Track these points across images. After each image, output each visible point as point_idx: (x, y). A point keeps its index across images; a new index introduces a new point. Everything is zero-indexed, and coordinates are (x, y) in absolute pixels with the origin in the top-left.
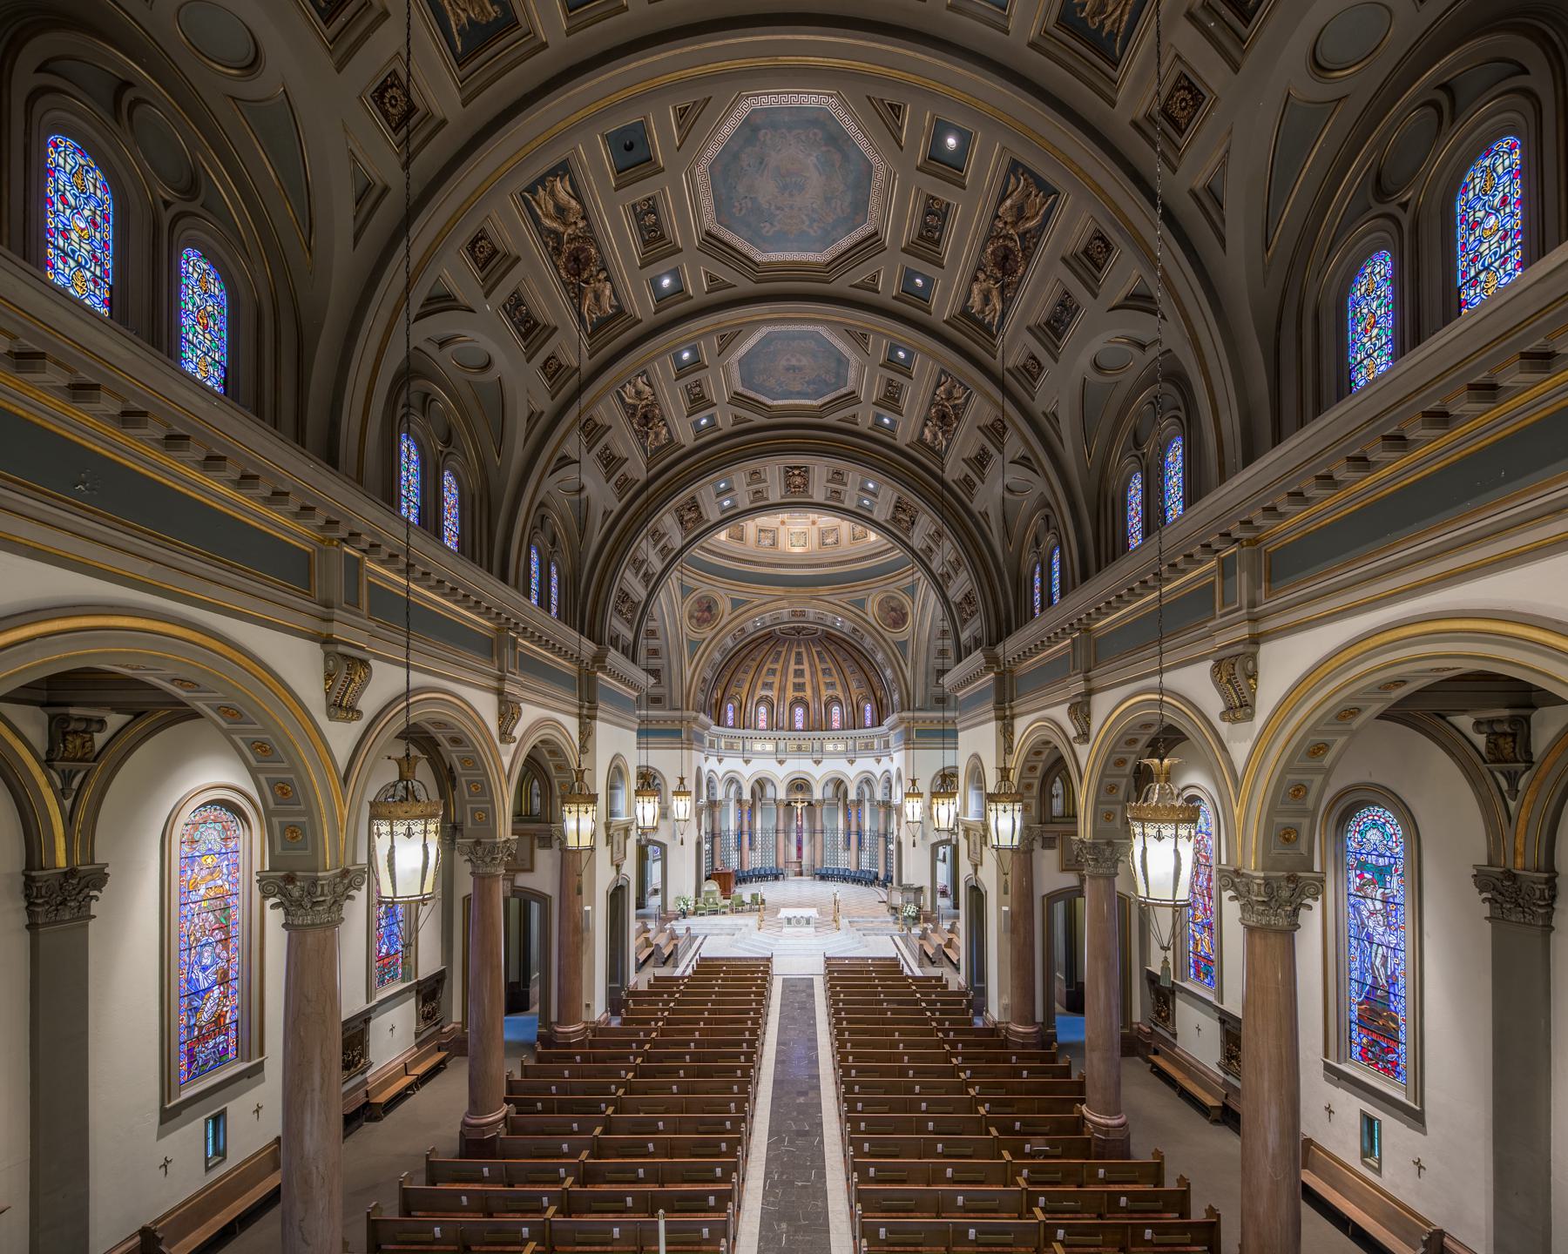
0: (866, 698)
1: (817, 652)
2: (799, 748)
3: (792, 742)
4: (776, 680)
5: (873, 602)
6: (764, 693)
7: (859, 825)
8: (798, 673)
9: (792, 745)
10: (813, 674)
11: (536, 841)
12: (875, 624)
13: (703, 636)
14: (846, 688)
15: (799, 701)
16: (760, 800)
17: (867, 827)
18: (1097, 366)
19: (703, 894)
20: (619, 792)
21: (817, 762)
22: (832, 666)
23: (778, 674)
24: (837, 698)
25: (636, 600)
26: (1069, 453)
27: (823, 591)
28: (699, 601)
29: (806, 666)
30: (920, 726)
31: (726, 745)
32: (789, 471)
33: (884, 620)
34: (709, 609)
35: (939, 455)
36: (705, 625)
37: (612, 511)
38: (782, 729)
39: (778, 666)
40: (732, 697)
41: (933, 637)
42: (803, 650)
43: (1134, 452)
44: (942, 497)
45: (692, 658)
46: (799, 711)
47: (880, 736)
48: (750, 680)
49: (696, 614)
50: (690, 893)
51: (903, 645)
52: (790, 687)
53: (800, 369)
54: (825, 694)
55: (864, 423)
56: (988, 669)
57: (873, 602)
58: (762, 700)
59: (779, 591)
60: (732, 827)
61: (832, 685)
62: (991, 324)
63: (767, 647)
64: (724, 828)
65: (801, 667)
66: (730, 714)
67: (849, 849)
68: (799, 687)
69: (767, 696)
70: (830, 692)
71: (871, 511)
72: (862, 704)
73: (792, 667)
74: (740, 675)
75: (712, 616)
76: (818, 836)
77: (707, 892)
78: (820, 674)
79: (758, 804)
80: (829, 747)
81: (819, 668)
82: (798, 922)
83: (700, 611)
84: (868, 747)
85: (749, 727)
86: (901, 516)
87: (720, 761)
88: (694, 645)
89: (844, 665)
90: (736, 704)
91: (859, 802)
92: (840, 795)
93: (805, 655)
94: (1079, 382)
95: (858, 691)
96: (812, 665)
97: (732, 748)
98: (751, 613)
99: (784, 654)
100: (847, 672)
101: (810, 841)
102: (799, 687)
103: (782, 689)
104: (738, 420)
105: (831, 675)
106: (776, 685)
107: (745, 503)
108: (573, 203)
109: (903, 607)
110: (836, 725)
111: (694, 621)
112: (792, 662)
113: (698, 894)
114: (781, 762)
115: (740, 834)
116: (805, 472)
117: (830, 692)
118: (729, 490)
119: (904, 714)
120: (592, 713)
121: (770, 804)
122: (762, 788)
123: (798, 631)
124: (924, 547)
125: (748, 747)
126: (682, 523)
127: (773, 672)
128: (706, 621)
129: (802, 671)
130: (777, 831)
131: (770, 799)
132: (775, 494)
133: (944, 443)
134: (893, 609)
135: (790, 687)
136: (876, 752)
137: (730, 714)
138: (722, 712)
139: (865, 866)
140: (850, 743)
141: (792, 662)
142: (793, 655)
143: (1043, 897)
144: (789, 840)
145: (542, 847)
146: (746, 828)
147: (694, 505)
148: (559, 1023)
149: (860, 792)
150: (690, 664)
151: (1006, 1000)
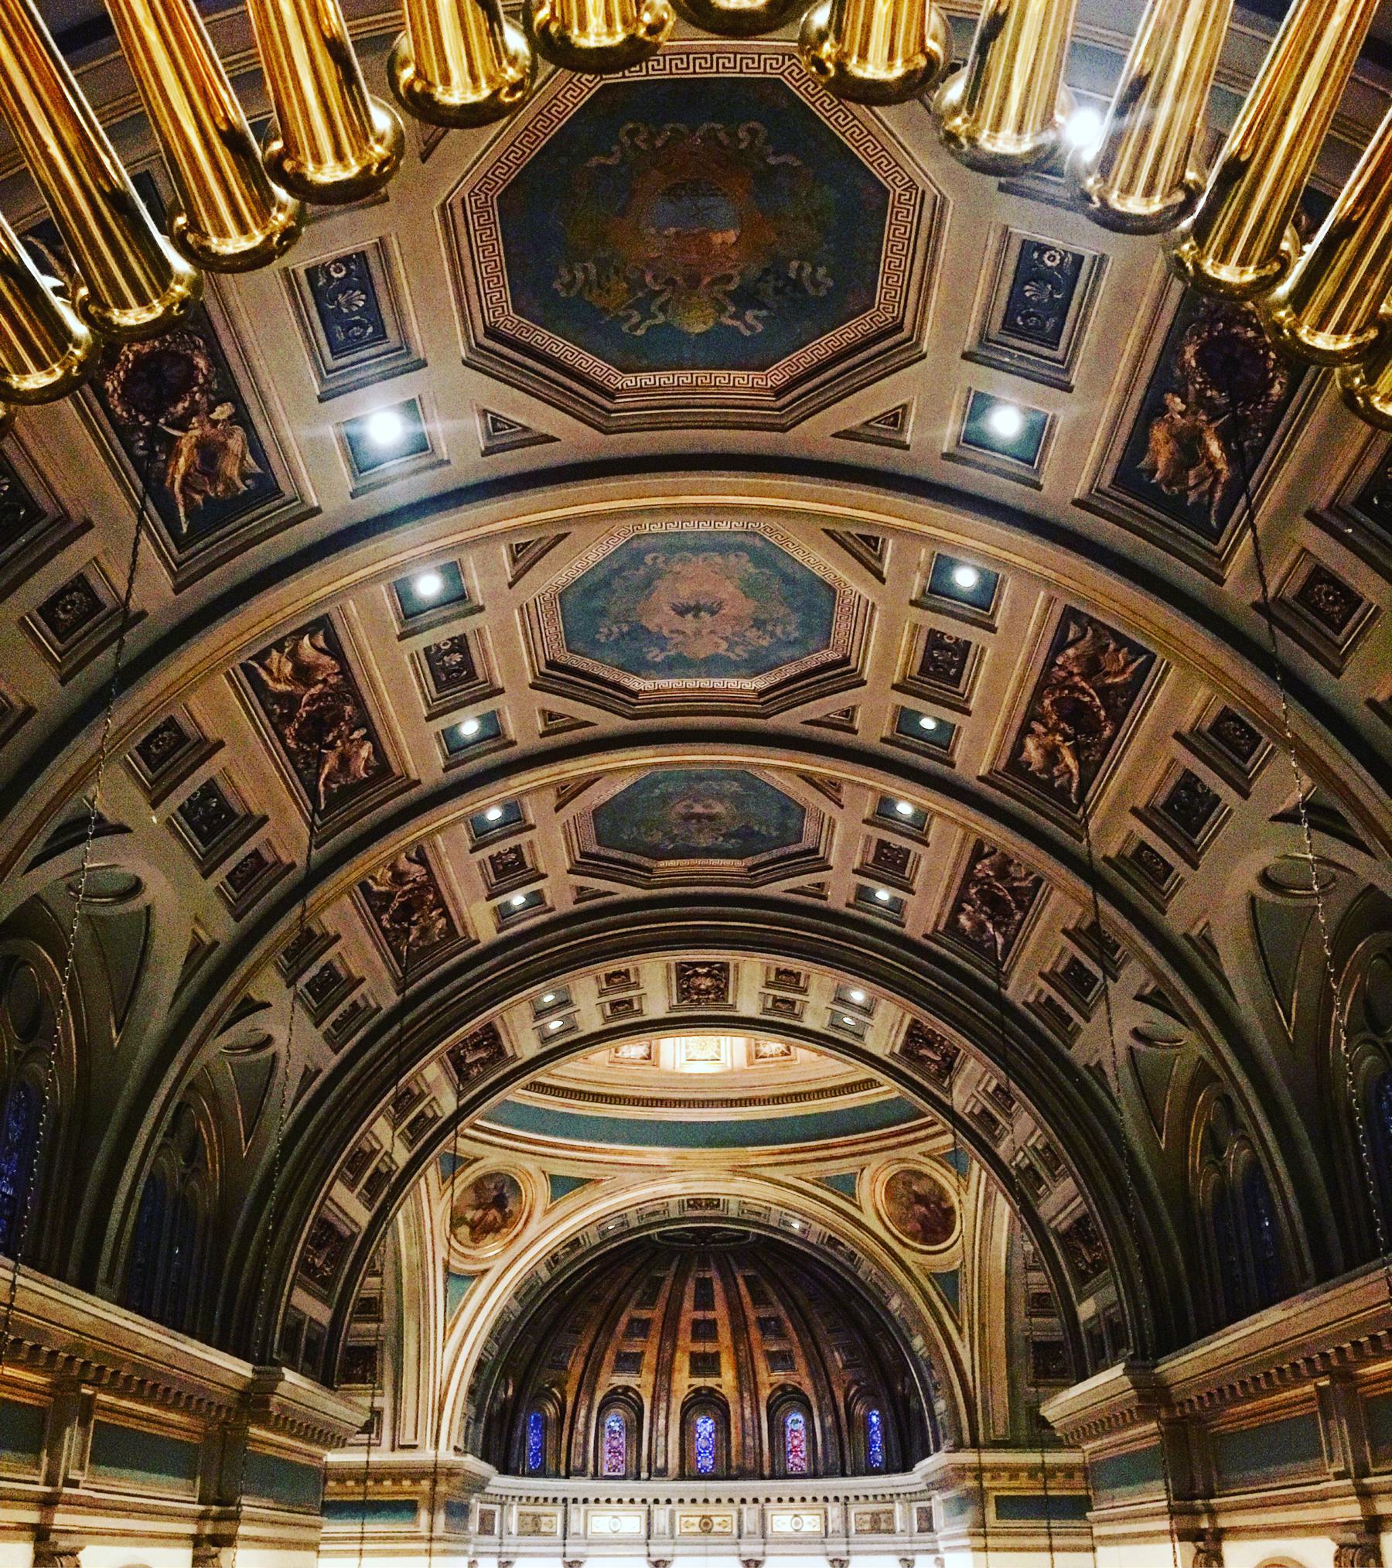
1: (746, 1279)
2: (706, 1524)
3: (688, 1508)
5: (874, 1180)
6: (620, 1380)
8: (705, 1330)
9: (688, 1519)
10: (739, 1330)
14: (819, 1369)
15: (704, 1401)
18: (1265, 879)
22: (783, 1313)
24: (796, 1390)
26: (1247, 1009)
28: (478, 1185)
29: (720, 1313)
30: (1002, 1487)
31: (522, 1523)
32: (685, 972)
33: (900, 1222)
34: (500, 1202)
35: (998, 964)
37: (319, 1071)
38: (662, 1473)
39: (655, 1314)
41: (1018, 1263)
42: (712, 1274)
43: (1368, 1034)
44: (1002, 1025)
46: (705, 1426)
47: (911, 1497)
48: (585, 1347)
49: (470, 1215)
51: (948, 1283)
52: (682, 1362)
53: (711, 818)
54: (769, 1379)
55: (839, 894)
56: (1146, 1411)
57: (874, 1180)
58: (619, 1397)
62: (1065, 790)
63: (628, 1271)
65: (710, 1315)
69: (627, 1389)
70: (779, 1377)
71: (861, 1037)
72: (859, 1410)
73: (689, 1313)
78: (755, 1334)
80: (781, 1522)
81: (751, 1315)
84: (879, 1524)
85: (581, 1472)
86: (923, 1052)
93: (717, 1287)
94: (1242, 908)
95: (848, 1376)
96: (735, 1309)
97: (537, 1532)
99: (668, 1282)
100: (821, 1330)
104: (582, 894)
105: (781, 1335)
106: (650, 1359)
107: (591, 1021)
108: (325, 660)
109: (942, 1195)
110: (798, 1460)
111: (464, 1231)
112: (688, 1304)
116: (720, 969)
117: (779, 1377)
118: (566, 1003)
120: (225, 1528)
124: (976, 1111)
125: (575, 1525)
126: (459, 1072)
127: (640, 1328)
128: (493, 1229)
129: (713, 1324)
132: (657, 1002)
133: (1000, 940)
134: (920, 1199)
135: (682, 1362)
136: (900, 1541)
140: (835, 1510)
142: (690, 1288)
147: (490, 1037)
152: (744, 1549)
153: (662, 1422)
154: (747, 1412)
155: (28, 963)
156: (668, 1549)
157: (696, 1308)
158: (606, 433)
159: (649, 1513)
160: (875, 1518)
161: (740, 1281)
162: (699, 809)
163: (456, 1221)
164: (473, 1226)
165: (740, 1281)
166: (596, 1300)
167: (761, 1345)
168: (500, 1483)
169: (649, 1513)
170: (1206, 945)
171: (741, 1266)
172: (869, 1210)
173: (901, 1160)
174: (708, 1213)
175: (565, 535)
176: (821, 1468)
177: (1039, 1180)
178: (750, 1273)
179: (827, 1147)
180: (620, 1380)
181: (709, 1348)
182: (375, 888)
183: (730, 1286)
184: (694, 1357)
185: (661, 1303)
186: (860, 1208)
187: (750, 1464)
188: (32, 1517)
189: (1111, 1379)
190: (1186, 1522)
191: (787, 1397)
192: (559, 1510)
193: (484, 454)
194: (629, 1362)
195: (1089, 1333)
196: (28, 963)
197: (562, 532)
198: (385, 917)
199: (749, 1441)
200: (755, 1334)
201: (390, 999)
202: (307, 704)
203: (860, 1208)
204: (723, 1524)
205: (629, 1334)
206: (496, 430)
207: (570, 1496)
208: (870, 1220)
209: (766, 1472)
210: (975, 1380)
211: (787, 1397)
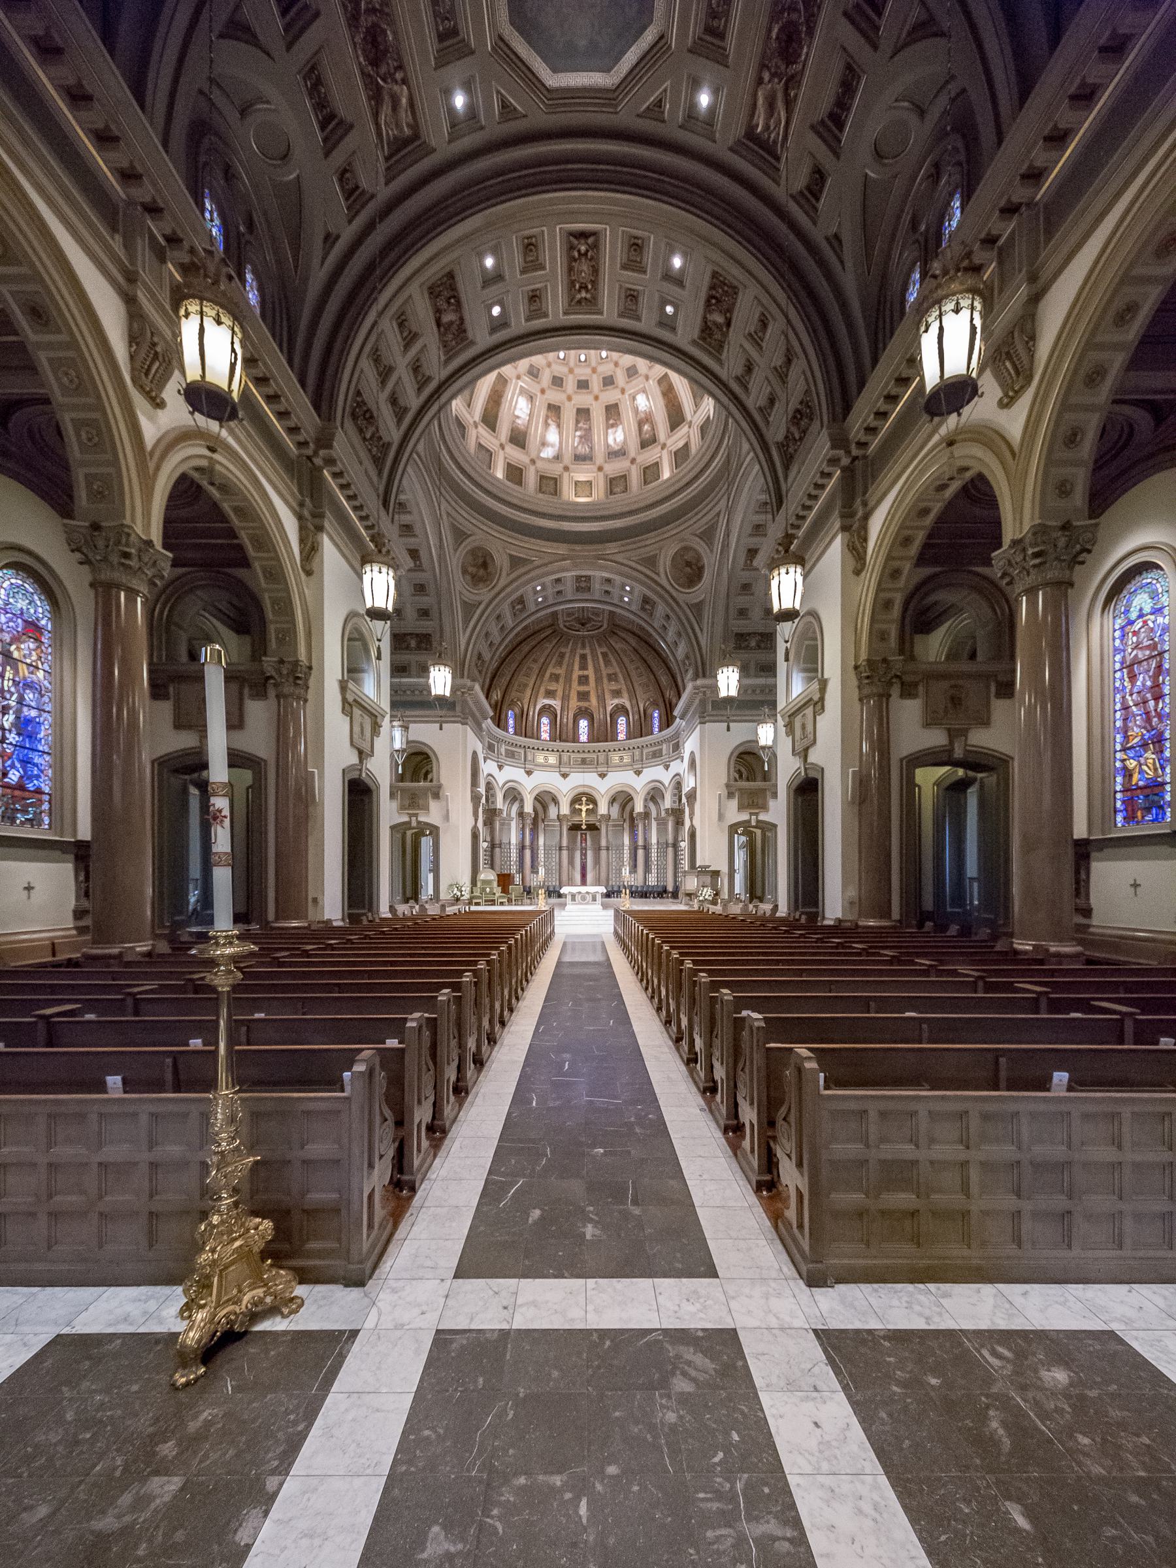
0: (655, 704)
4: (559, 688)
6: (547, 701)
7: (645, 839)
8: (584, 680)
10: (599, 680)
11: (246, 691)
12: (669, 587)
13: (478, 598)
14: (633, 695)
16: (543, 821)
17: (654, 840)
19: (479, 884)
20: (365, 675)
21: (603, 776)
22: (618, 670)
23: (562, 680)
24: (623, 707)
25: (386, 439)
27: (612, 548)
28: (474, 552)
29: (590, 672)
34: (485, 565)
36: (481, 585)
39: (560, 671)
40: (512, 704)
42: (587, 651)
45: (466, 621)
46: (583, 724)
49: (470, 569)
50: (465, 879)
52: (574, 696)
54: (611, 703)
59: (562, 549)
60: (514, 841)
61: (617, 693)
64: (505, 841)
65: (586, 673)
66: (511, 722)
67: (635, 872)
68: (584, 696)
69: (550, 706)
70: (616, 701)
71: (673, 329)
72: (649, 711)
73: (577, 673)
74: (521, 678)
75: (489, 574)
76: (603, 853)
77: (484, 882)
78: (605, 681)
79: (541, 826)
82: (584, 898)
83: (474, 566)
84: (657, 754)
87: (500, 767)
88: (469, 608)
89: (631, 667)
90: (517, 710)
91: (646, 815)
92: (626, 815)
93: (589, 658)
96: (597, 670)
98: (533, 574)
99: (567, 655)
101: (594, 867)
102: (584, 696)
103: (568, 680)
105: (616, 681)
106: (560, 693)
111: (468, 577)
112: (576, 666)
113: (474, 882)
114: (565, 776)
115: (522, 848)
117: (616, 701)
119: (699, 682)
122: (545, 808)
123: (583, 620)
125: (530, 757)
127: (555, 678)
129: (587, 677)
130: (560, 849)
131: (553, 820)
134: (688, 564)
135: (574, 696)
137: (511, 722)
138: (503, 717)
139: (652, 881)
140: (637, 752)
141: (576, 666)
142: (577, 659)
143: (901, 760)
144: (573, 867)
145: (253, 697)
146: (527, 842)
148: (277, 919)
150: (465, 630)
151: (853, 892)
164: (473, 576)
166: (535, 661)
167: (608, 686)
171: (600, 646)
172: (663, 575)
180: (547, 701)
183: (594, 656)
184: (579, 693)
185: (564, 666)
191: (621, 710)
192: (522, 751)
194: (550, 694)
200: (605, 681)
208: (664, 583)
210: (726, 497)
211: (621, 710)
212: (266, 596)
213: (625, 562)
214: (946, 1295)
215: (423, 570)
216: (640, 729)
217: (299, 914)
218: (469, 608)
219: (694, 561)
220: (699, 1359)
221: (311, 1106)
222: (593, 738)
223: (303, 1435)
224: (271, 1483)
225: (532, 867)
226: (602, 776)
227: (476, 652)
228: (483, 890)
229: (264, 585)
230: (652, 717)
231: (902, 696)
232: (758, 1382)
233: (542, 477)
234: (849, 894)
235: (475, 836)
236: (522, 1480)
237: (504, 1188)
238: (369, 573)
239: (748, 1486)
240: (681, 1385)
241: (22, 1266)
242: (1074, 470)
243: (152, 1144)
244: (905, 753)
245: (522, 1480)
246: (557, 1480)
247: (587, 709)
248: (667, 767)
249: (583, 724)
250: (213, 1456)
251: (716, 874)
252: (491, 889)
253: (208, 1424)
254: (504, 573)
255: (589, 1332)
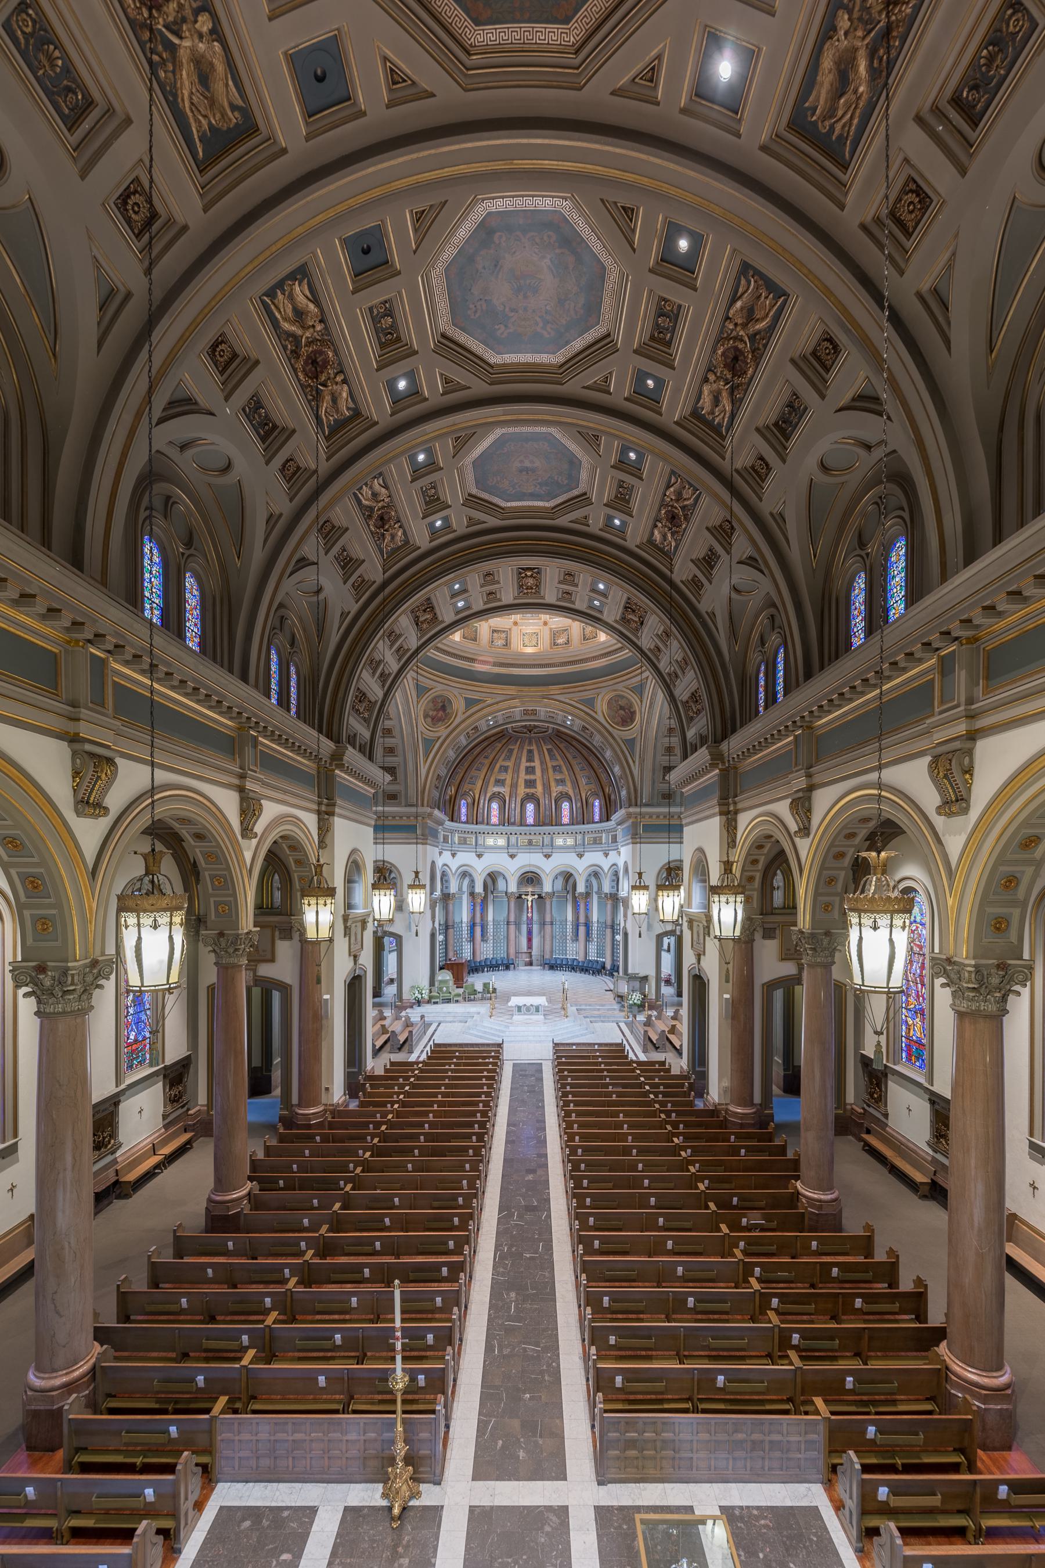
0: (595, 795)
1: (548, 750)
2: (530, 843)
4: (508, 777)
6: (496, 789)
7: (587, 917)
8: (530, 770)
9: (523, 840)
10: (544, 771)
11: (277, 933)
14: (576, 784)
15: (530, 798)
16: (492, 892)
17: (595, 919)
18: (824, 467)
20: (356, 885)
22: (562, 763)
23: (510, 771)
24: (567, 794)
25: (373, 700)
27: (554, 690)
28: (434, 700)
29: (537, 764)
30: (647, 821)
34: (443, 708)
38: (514, 824)
39: (510, 764)
40: (466, 794)
42: (534, 747)
45: (427, 755)
46: (530, 807)
47: (608, 831)
48: (482, 777)
49: (431, 713)
50: (425, 983)
51: (631, 743)
53: (533, 470)
54: (556, 790)
55: (595, 525)
58: (495, 796)
59: (511, 690)
61: (562, 782)
62: (720, 425)
64: (457, 920)
65: (532, 764)
67: (577, 940)
68: (531, 784)
69: (499, 793)
71: (601, 612)
72: (590, 800)
73: (524, 764)
74: (473, 772)
77: (441, 982)
78: (550, 771)
79: (490, 897)
80: (559, 841)
81: (549, 765)
84: (597, 841)
85: (482, 823)
88: (429, 743)
90: (470, 800)
91: (588, 895)
93: (536, 753)
95: (587, 787)
96: (543, 763)
97: (465, 843)
100: (577, 769)
101: (540, 932)
102: (531, 784)
104: (471, 521)
105: (561, 772)
106: (508, 782)
107: (479, 605)
109: (631, 705)
110: (566, 820)
111: (429, 720)
112: (524, 759)
113: (432, 983)
114: (512, 856)
115: (472, 926)
117: (560, 788)
118: (465, 591)
119: (631, 810)
120: (330, 809)
121: (501, 897)
123: (530, 729)
125: (480, 842)
127: (505, 769)
128: (440, 720)
129: (533, 768)
130: (508, 923)
132: (508, 595)
133: (673, 544)
134: (622, 708)
137: (464, 810)
139: (593, 956)
140: (579, 837)
141: (524, 759)
142: (525, 752)
144: (520, 932)
146: (478, 920)
147: (429, 606)
149: (589, 885)
151: (726, 1083)
152: (544, 851)
153: (513, 805)
154: (547, 802)
155: (177, 503)
156: (516, 851)
157: (527, 761)
158: (466, 90)
159: (508, 838)
160: (595, 839)
161: (545, 751)
162: (527, 464)
163: (426, 716)
165: (545, 751)
166: (486, 757)
168: (448, 824)
169: (508, 838)
170: (780, 518)
173: (615, 690)
174: (532, 717)
175: (475, 433)
176: (575, 822)
177: (677, 676)
178: (550, 747)
179: (583, 686)
180: (496, 789)
181: (532, 777)
182: (364, 501)
184: (526, 781)
186: (596, 713)
187: (547, 821)
188: (236, 781)
189: (703, 755)
190: (725, 808)
191: (564, 796)
193: (388, 107)
194: (500, 782)
195: (691, 744)
196: (177, 503)
197: (473, 431)
198: (371, 523)
199: (547, 813)
201: (379, 578)
202: (306, 346)
203: (596, 713)
204: (537, 842)
205: (500, 771)
206: (394, 83)
207: (478, 831)
209: (554, 823)
212: (296, 874)
213: (567, 701)
214: (645, 1489)
215: (391, 719)
216: (582, 817)
217: (316, 1102)
218: (429, 743)
219: (627, 707)
220: (554, 1518)
221: (421, 1421)
222: (538, 823)
223: (437, 1545)
224: (433, 1560)
225: (482, 935)
226: (547, 856)
227: (436, 775)
228: (441, 989)
229: (294, 868)
230: (593, 805)
231: (764, 937)
232: (571, 1527)
233: (494, 631)
234: (724, 1085)
235: (433, 936)
236: (500, 1560)
237: (487, 1423)
238: (377, 896)
239: (561, 1562)
240: (547, 1529)
241: (319, 1476)
242: (832, 898)
243: (365, 1433)
244: (766, 979)
245: (500, 1560)
246: (510, 1560)
247: (533, 794)
248: (606, 855)
249: (530, 807)
250: (414, 1552)
251: (645, 978)
252: (447, 988)
253: (409, 1541)
254: (460, 713)
255: (519, 1507)
